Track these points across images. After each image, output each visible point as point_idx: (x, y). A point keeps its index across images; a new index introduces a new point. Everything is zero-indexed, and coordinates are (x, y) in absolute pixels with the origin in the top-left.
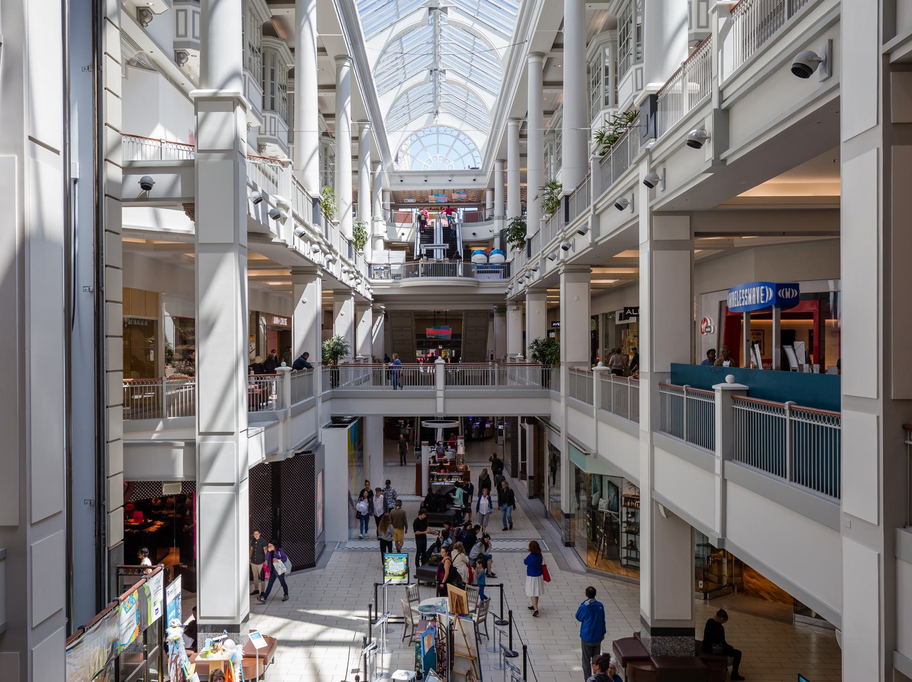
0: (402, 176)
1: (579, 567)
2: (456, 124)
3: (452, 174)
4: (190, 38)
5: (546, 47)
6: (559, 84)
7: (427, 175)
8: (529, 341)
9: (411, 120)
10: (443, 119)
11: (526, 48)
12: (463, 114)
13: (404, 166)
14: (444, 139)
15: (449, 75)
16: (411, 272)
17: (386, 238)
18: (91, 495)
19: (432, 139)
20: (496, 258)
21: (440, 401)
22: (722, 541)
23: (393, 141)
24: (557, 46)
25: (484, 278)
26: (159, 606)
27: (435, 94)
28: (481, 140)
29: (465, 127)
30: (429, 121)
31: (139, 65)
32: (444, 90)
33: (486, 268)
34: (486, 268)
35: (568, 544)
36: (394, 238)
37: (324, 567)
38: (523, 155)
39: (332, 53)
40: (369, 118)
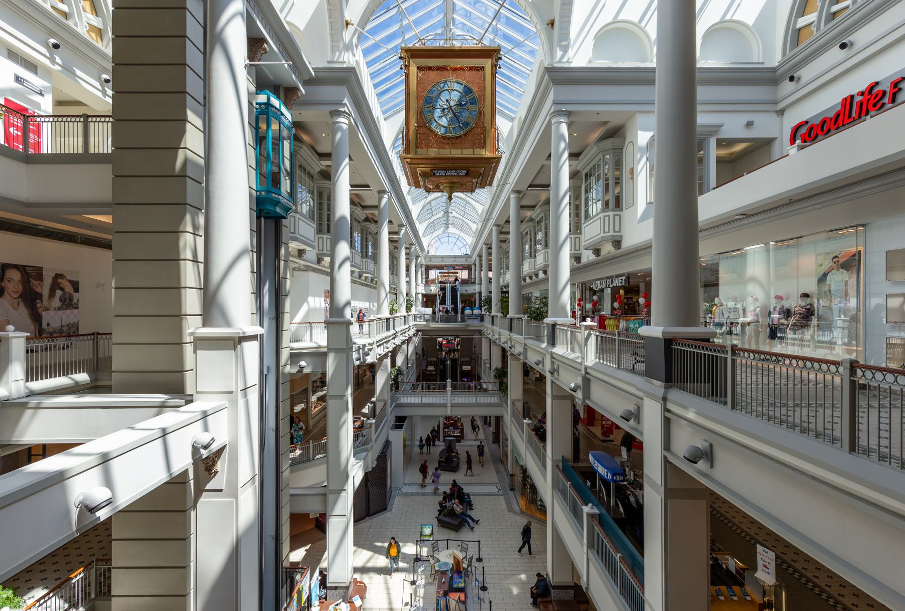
0: (431, 258)
1: (517, 509)
2: (458, 232)
3: (455, 257)
4: (325, 251)
5: (502, 222)
6: (508, 233)
7: (443, 257)
8: (493, 368)
9: (435, 230)
10: (451, 230)
11: (491, 222)
12: (462, 227)
13: (432, 253)
14: (451, 240)
15: (454, 214)
16: (434, 320)
17: (424, 292)
18: (273, 533)
19: (446, 239)
20: (476, 312)
21: (449, 408)
22: (587, 588)
23: (425, 241)
24: (508, 222)
25: (471, 322)
26: (307, 590)
27: (447, 220)
28: (470, 240)
29: (462, 235)
30: (444, 232)
31: (299, 269)
32: (451, 219)
33: (472, 317)
34: (472, 317)
35: (512, 489)
36: (428, 292)
37: (391, 510)
38: (490, 254)
39: (396, 224)
40: (414, 241)
